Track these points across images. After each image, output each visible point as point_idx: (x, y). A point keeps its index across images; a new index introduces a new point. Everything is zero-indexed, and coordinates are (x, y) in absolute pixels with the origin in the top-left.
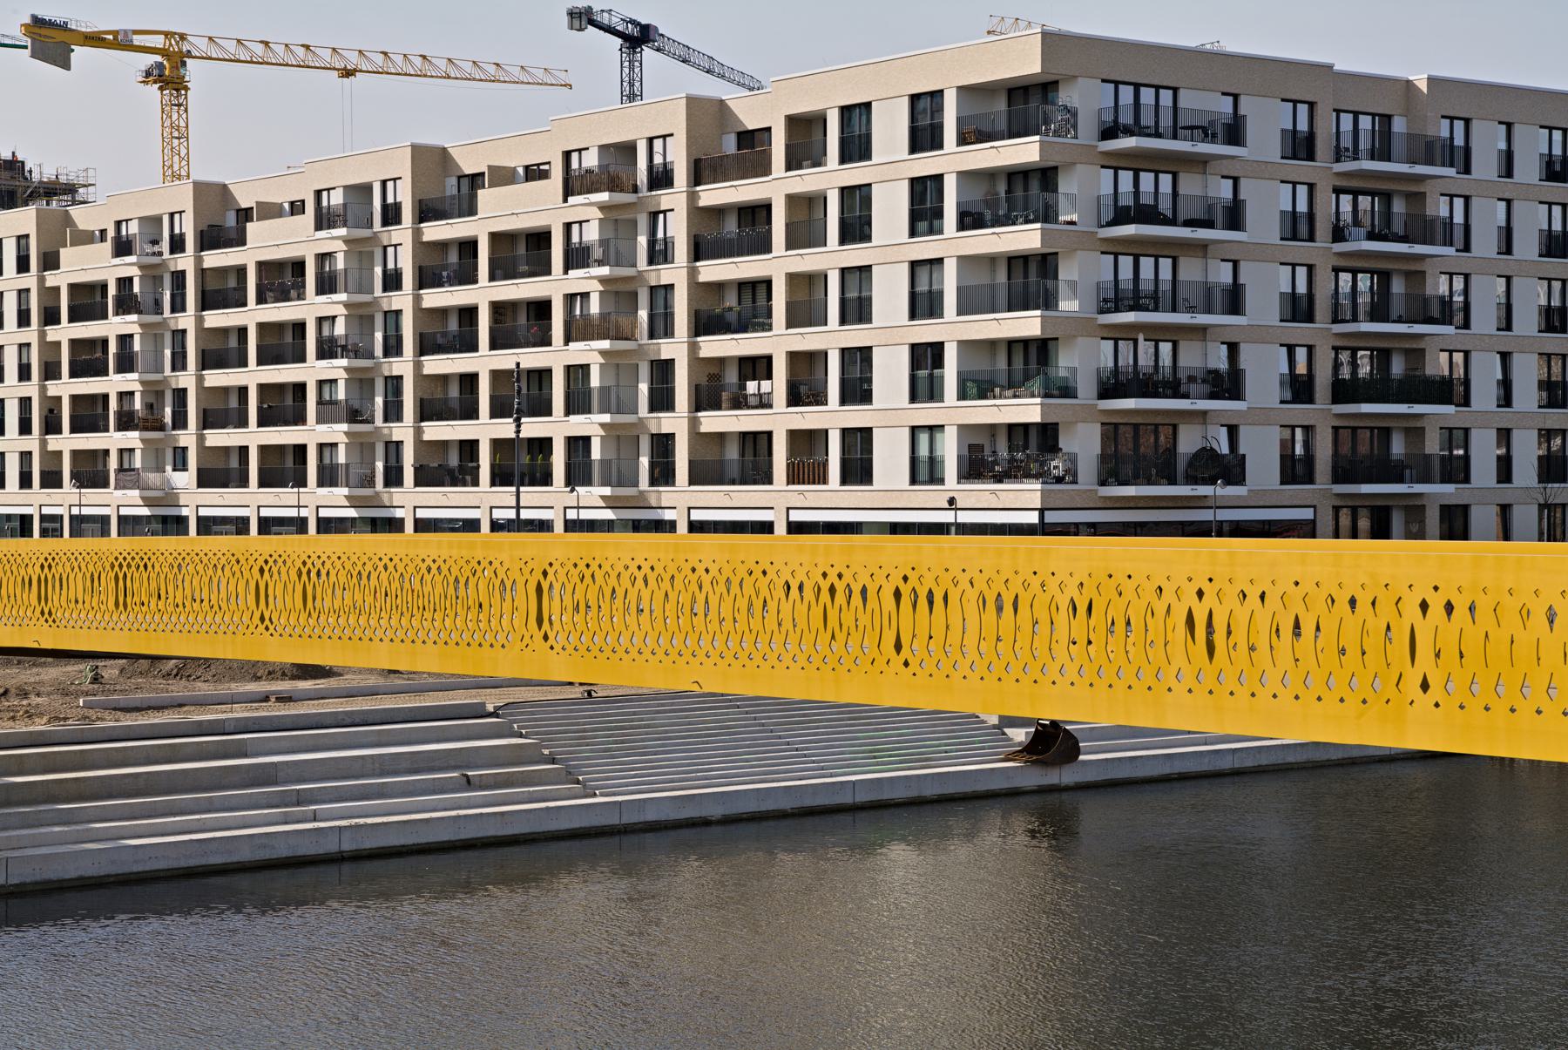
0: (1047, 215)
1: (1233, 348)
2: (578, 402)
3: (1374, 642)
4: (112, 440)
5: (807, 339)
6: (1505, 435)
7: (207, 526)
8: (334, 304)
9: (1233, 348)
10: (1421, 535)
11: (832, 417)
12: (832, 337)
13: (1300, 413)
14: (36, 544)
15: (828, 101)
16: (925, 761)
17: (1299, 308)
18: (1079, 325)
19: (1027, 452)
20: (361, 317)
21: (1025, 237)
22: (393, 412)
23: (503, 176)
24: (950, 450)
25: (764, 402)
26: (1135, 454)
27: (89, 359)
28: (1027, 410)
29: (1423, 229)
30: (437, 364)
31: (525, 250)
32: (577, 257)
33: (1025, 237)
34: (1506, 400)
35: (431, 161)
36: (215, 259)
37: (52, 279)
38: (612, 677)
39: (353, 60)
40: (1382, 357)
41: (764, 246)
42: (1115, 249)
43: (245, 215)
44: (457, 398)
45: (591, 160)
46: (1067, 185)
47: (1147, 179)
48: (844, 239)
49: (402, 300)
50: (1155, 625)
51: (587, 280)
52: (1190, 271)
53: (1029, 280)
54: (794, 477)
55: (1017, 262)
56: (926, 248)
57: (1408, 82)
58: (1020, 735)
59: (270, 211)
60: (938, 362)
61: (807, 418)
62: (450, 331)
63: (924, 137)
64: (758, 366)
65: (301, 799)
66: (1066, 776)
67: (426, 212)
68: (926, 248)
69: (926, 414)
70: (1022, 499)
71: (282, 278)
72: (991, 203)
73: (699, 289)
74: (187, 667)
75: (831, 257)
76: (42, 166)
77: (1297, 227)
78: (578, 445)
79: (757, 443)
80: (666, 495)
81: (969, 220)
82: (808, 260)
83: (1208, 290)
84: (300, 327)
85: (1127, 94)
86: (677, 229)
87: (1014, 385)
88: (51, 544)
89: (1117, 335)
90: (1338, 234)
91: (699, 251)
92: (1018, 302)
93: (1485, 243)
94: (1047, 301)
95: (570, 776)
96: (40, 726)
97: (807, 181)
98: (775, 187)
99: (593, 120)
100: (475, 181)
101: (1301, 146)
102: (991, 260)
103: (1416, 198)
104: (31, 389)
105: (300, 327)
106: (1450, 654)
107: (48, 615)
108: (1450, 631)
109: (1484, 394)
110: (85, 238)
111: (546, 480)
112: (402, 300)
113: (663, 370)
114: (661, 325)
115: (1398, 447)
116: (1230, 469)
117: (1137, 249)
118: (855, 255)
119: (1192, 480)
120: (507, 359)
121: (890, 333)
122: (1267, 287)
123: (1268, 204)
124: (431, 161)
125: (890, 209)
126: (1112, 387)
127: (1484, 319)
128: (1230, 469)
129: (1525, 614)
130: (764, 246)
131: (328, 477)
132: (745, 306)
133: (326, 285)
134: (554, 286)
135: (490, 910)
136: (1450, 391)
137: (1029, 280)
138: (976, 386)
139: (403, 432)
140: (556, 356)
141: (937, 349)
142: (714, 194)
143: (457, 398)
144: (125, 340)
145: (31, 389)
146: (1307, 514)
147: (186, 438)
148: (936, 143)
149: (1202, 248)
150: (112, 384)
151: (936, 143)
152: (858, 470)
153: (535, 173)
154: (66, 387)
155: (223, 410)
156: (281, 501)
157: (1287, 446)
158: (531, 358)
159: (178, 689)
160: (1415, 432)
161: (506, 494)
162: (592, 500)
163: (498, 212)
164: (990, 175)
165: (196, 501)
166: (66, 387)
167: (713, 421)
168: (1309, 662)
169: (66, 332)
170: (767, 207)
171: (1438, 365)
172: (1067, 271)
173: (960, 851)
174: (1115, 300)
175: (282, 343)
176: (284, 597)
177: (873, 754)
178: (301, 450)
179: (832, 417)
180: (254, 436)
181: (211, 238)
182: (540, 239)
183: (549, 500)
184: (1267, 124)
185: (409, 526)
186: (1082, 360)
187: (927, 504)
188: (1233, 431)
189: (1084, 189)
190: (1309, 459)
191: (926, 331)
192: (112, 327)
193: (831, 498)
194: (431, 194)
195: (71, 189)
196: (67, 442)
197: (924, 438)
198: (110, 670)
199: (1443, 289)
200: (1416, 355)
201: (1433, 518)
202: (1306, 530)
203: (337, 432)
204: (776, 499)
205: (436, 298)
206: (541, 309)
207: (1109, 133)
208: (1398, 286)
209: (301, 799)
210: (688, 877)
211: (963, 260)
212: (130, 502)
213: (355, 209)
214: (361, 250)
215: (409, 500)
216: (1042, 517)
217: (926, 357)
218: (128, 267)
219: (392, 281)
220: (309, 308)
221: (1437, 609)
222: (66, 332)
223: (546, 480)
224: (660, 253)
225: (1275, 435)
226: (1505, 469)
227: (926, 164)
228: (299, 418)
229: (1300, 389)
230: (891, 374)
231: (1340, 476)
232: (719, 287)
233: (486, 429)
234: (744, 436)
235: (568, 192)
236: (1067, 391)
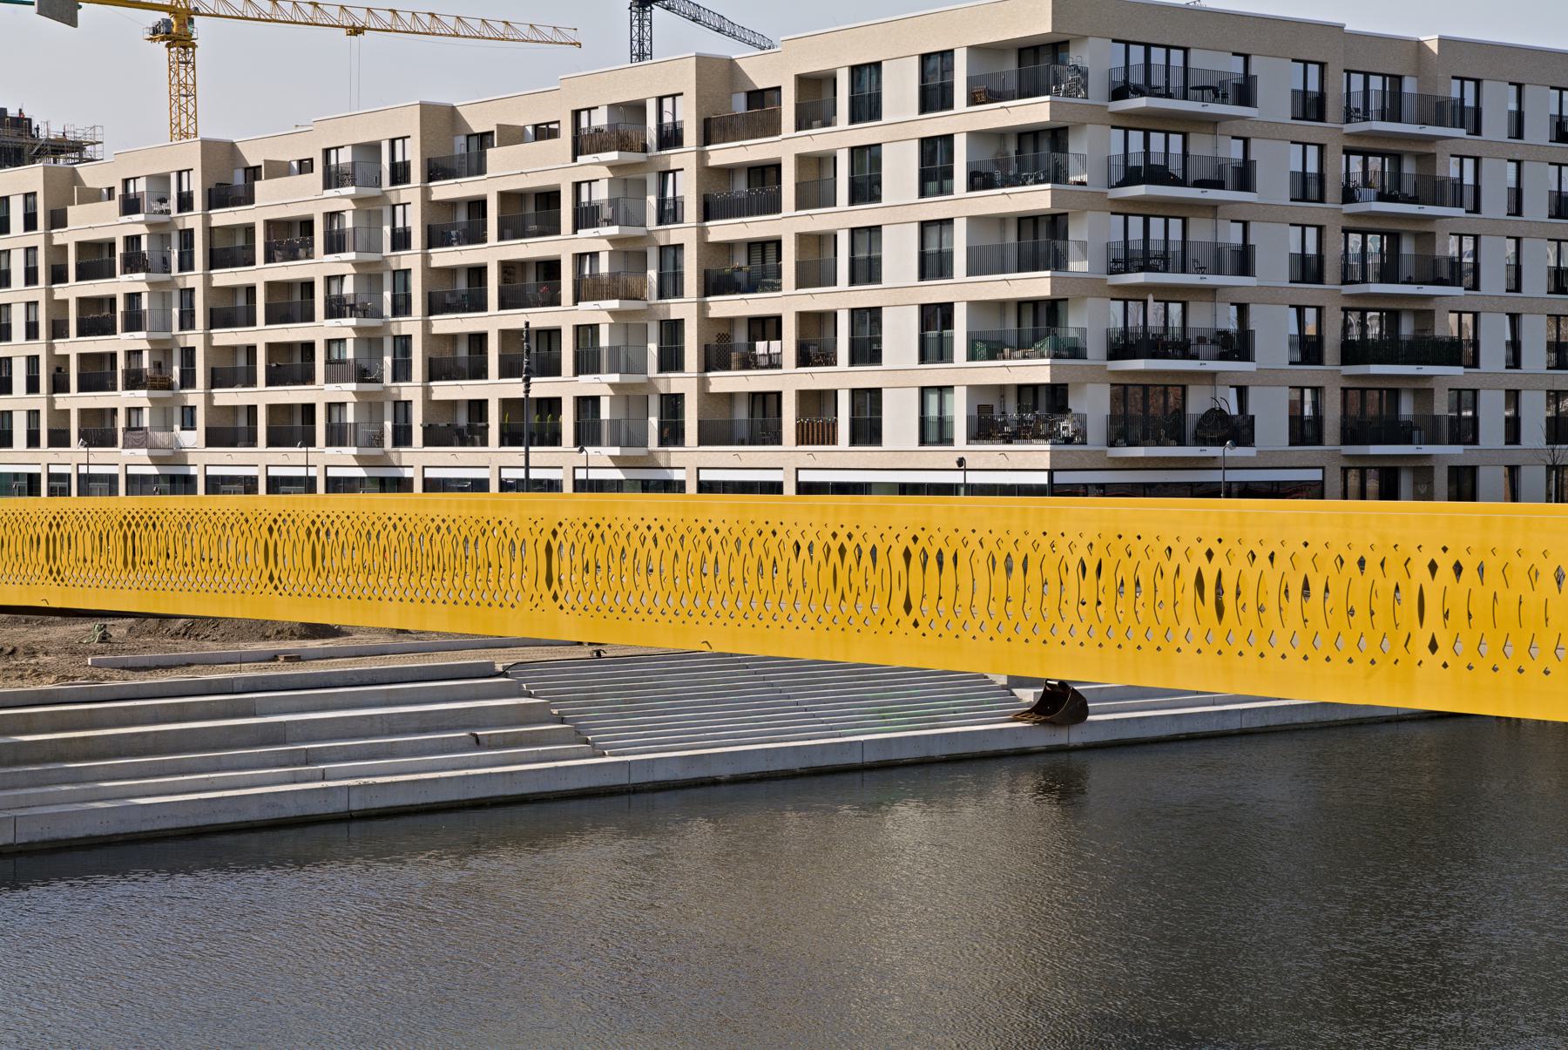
0: (1057, 175)
1: (1242, 309)
2: (587, 362)
3: (1383, 603)
4: (120, 399)
5: (817, 299)
6: (1513, 397)
7: (216, 485)
8: (343, 264)
9: (1242, 309)
10: (1429, 497)
11: (842, 377)
12: (841, 298)
13: (1309, 374)
14: (44, 503)
15: (839, 60)
16: (934, 721)
17: (1308, 269)
18: (1089, 286)
19: (1037, 411)
20: (370, 276)
21: (1036, 198)
22: (402, 371)
23: (511, 135)
24: (959, 411)
25: (774, 363)
26: (1144, 416)
27: (96, 317)
28: (1037, 371)
29: (1434, 190)
30: (445, 324)
31: (535, 210)
32: (586, 217)
33: (1036, 198)
34: (1515, 361)
35: (717, 75)
36: (224, 217)
37: (59, 237)
38: (622, 636)
39: (361, 18)
40: (1392, 318)
41: (774, 206)
42: (1125, 210)
43: (253, 173)
44: (463, 359)
45: (600, 119)
46: (1077, 146)
47: (1157, 140)
48: (854, 118)
49: (410, 260)
50: (1165, 585)
51: (596, 239)
52: (1200, 231)
53: (1039, 240)
54: (802, 439)
55: (1027, 222)
56: (936, 208)
57: (1419, 42)
58: (1028, 696)
59: (278, 169)
60: (948, 322)
61: (816, 378)
62: (463, 290)
63: (934, 97)
64: (768, 326)
65: (310, 758)
66: (1074, 736)
67: (434, 171)
68: (936, 208)
69: (935, 374)
70: (1030, 460)
71: (290, 237)
72: (1002, 163)
73: (709, 249)
74: (196, 626)
75: (841, 217)
76: (49, 123)
77: (1308, 188)
78: (588, 405)
79: (767, 403)
80: (675, 455)
81: (979, 180)
82: (817, 220)
83: (1218, 250)
84: (308, 286)
85: (1137, 54)
86: (687, 188)
87: (1023, 346)
88: (59, 502)
89: (1127, 296)
90: (1348, 195)
91: (709, 211)
92: (1028, 262)
93: (1495, 204)
94: (1057, 262)
95: (579, 736)
96: (47, 685)
97: (817, 140)
98: (786, 146)
99: (605, 83)
100: (484, 139)
101: (1311, 107)
102: (1001, 220)
103: (1426, 159)
104: (39, 348)
105: (308, 286)
106: (1458, 615)
107: (56, 574)
108: (1361, 583)
109: (1493, 356)
110: (93, 196)
111: (555, 440)
112: (410, 260)
113: (672, 330)
114: (671, 285)
115: (1407, 408)
116: (1239, 430)
117: (1147, 210)
118: (865, 134)
119: (1201, 441)
120: (516, 319)
121: (900, 293)
122: (1278, 245)
123: (1278, 163)
124: (440, 120)
125: (900, 170)
126: (1121, 348)
127: (1494, 280)
128: (1239, 430)
129: (1534, 575)
130: (774, 206)
131: (336, 436)
132: (754, 266)
133: (335, 244)
134: (563, 246)
135: (503, 867)
136: (1459, 352)
137: (1039, 240)
138: (986, 347)
139: (411, 391)
140: (565, 316)
141: (947, 310)
142: (724, 154)
143: (463, 359)
144: (133, 298)
145: (39, 348)
146: (1316, 475)
147: (195, 397)
148: (946, 103)
149: (1212, 208)
150: (120, 342)
151: (946, 103)
152: (867, 430)
153: (544, 132)
154: (74, 346)
155: (231, 369)
156: (289, 461)
157: (1296, 407)
158: (540, 318)
159: (186, 648)
160: (1424, 394)
161: (515, 454)
162: (601, 460)
163: (510, 170)
164: (1000, 135)
165: (203, 459)
166: (74, 346)
167: (725, 382)
168: (1317, 622)
169: (73, 290)
170: (776, 167)
171: (1448, 326)
172: (1077, 232)
173: (969, 811)
174: (1124, 261)
175: (291, 302)
176: (294, 557)
177: (881, 714)
178: (309, 409)
179: (842, 377)
180: (262, 396)
181: (219, 196)
182: (548, 199)
183: (558, 460)
184: (1278, 85)
185: (418, 486)
186: (1093, 321)
187: (936, 465)
188: (1242, 392)
189: (1094, 150)
190: (1318, 420)
191: (936, 292)
192: (120, 285)
193: (840, 459)
194: (439, 153)
195: (78, 147)
196: (75, 401)
197: (933, 399)
198: (118, 629)
199: (1453, 250)
200: (1425, 316)
201: (1441, 479)
202: (1316, 491)
203: (346, 391)
204: (786, 459)
205: (444, 257)
206: (550, 268)
207: (1119, 93)
208: (1407, 247)
209: (310, 758)
210: (698, 837)
211: (973, 220)
212: (138, 461)
213: (364, 167)
214: (370, 209)
215: (418, 460)
216: (1051, 478)
217: (936, 317)
218: (136, 225)
219: (401, 240)
220: (318, 266)
221: (1469, 572)
222: (73, 290)
223: (555, 440)
224: (669, 213)
225: (1284, 396)
226: (1513, 431)
227: (936, 124)
228: (308, 378)
229: (1309, 350)
230: (900, 334)
231: (1349, 437)
232: (728, 247)
233: (495, 389)
234: (753, 396)
235: (577, 151)
236: (1077, 352)
